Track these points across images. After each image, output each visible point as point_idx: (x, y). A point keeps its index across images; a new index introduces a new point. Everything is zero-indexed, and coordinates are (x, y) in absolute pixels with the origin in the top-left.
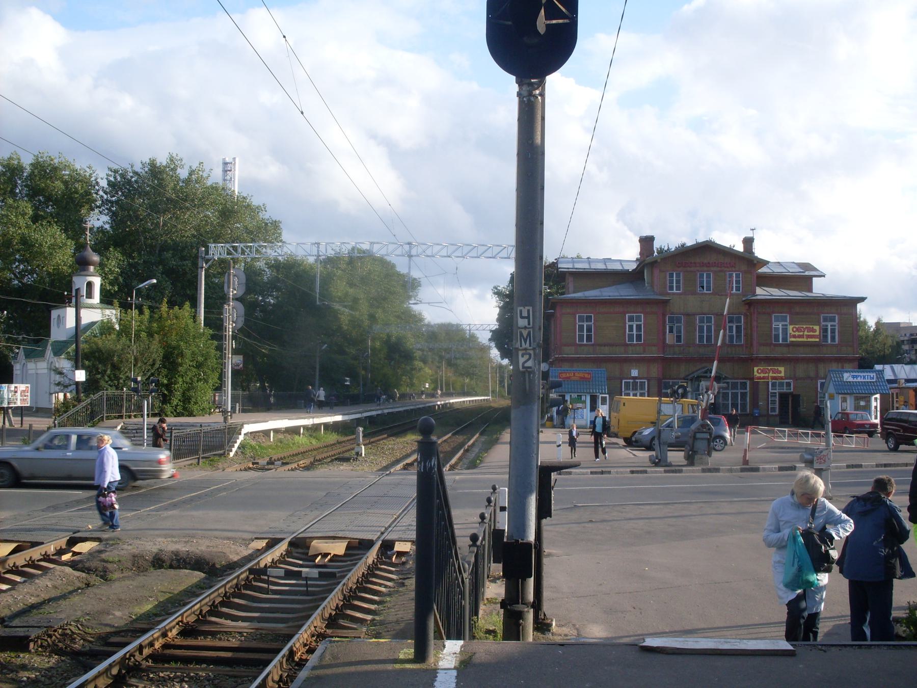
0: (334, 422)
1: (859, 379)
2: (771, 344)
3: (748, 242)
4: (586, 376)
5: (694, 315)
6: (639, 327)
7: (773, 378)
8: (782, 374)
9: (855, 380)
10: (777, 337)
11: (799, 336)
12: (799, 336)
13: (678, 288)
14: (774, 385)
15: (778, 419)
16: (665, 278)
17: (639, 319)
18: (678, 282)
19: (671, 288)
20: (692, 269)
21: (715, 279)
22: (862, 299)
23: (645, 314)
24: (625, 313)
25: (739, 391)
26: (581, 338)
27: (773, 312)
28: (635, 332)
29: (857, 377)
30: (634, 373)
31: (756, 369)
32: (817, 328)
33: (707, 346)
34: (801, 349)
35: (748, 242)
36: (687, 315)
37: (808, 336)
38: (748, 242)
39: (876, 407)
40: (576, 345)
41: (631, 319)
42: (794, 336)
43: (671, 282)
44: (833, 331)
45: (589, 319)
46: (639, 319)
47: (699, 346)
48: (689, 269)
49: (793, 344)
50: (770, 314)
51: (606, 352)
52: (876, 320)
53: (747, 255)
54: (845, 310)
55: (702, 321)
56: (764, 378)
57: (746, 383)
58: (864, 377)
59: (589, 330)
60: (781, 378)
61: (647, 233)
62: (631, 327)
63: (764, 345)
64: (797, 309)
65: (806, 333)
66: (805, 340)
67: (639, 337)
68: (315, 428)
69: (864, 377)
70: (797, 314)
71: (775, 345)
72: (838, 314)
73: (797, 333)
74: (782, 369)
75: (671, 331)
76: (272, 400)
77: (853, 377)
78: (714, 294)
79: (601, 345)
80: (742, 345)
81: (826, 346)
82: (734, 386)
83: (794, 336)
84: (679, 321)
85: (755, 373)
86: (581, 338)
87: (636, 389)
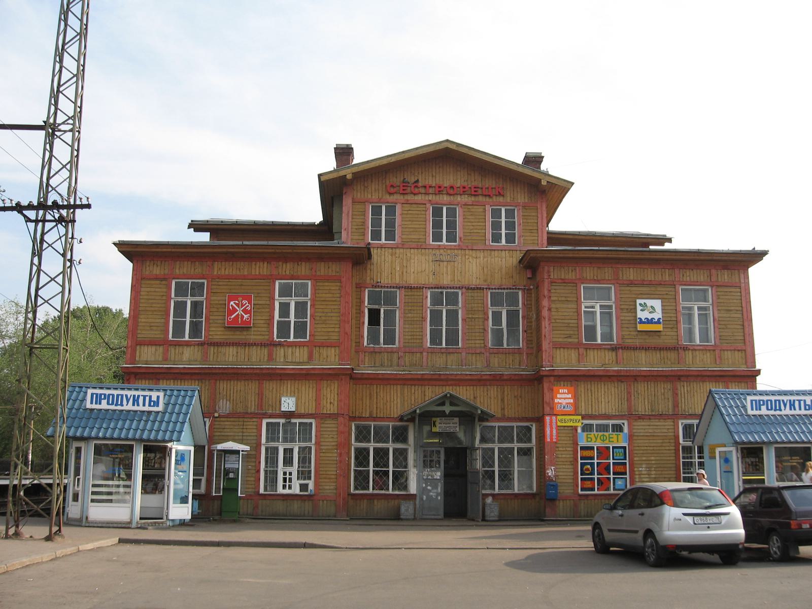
5: (420, 288)
6: (301, 308)
10: (591, 330)
16: (364, 213)
19: (376, 235)
20: (418, 198)
22: (756, 256)
23: (315, 279)
24: (272, 278)
25: (391, 446)
26: (179, 328)
27: (583, 280)
28: (292, 318)
30: (288, 404)
33: (447, 352)
43: (496, 226)
45: (197, 289)
47: (431, 352)
48: (410, 197)
50: (575, 284)
53: (528, 171)
54: (725, 276)
55: (437, 300)
57: (529, 429)
58: (136, 401)
61: (344, 141)
62: (285, 308)
69: (136, 401)
70: (631, 283)
72: (712, 286)
76: (429, 488)
80: (519, 351)
81: (694, 349)
82: (381, 435)
86: (179, 328)
87: (293, 440)
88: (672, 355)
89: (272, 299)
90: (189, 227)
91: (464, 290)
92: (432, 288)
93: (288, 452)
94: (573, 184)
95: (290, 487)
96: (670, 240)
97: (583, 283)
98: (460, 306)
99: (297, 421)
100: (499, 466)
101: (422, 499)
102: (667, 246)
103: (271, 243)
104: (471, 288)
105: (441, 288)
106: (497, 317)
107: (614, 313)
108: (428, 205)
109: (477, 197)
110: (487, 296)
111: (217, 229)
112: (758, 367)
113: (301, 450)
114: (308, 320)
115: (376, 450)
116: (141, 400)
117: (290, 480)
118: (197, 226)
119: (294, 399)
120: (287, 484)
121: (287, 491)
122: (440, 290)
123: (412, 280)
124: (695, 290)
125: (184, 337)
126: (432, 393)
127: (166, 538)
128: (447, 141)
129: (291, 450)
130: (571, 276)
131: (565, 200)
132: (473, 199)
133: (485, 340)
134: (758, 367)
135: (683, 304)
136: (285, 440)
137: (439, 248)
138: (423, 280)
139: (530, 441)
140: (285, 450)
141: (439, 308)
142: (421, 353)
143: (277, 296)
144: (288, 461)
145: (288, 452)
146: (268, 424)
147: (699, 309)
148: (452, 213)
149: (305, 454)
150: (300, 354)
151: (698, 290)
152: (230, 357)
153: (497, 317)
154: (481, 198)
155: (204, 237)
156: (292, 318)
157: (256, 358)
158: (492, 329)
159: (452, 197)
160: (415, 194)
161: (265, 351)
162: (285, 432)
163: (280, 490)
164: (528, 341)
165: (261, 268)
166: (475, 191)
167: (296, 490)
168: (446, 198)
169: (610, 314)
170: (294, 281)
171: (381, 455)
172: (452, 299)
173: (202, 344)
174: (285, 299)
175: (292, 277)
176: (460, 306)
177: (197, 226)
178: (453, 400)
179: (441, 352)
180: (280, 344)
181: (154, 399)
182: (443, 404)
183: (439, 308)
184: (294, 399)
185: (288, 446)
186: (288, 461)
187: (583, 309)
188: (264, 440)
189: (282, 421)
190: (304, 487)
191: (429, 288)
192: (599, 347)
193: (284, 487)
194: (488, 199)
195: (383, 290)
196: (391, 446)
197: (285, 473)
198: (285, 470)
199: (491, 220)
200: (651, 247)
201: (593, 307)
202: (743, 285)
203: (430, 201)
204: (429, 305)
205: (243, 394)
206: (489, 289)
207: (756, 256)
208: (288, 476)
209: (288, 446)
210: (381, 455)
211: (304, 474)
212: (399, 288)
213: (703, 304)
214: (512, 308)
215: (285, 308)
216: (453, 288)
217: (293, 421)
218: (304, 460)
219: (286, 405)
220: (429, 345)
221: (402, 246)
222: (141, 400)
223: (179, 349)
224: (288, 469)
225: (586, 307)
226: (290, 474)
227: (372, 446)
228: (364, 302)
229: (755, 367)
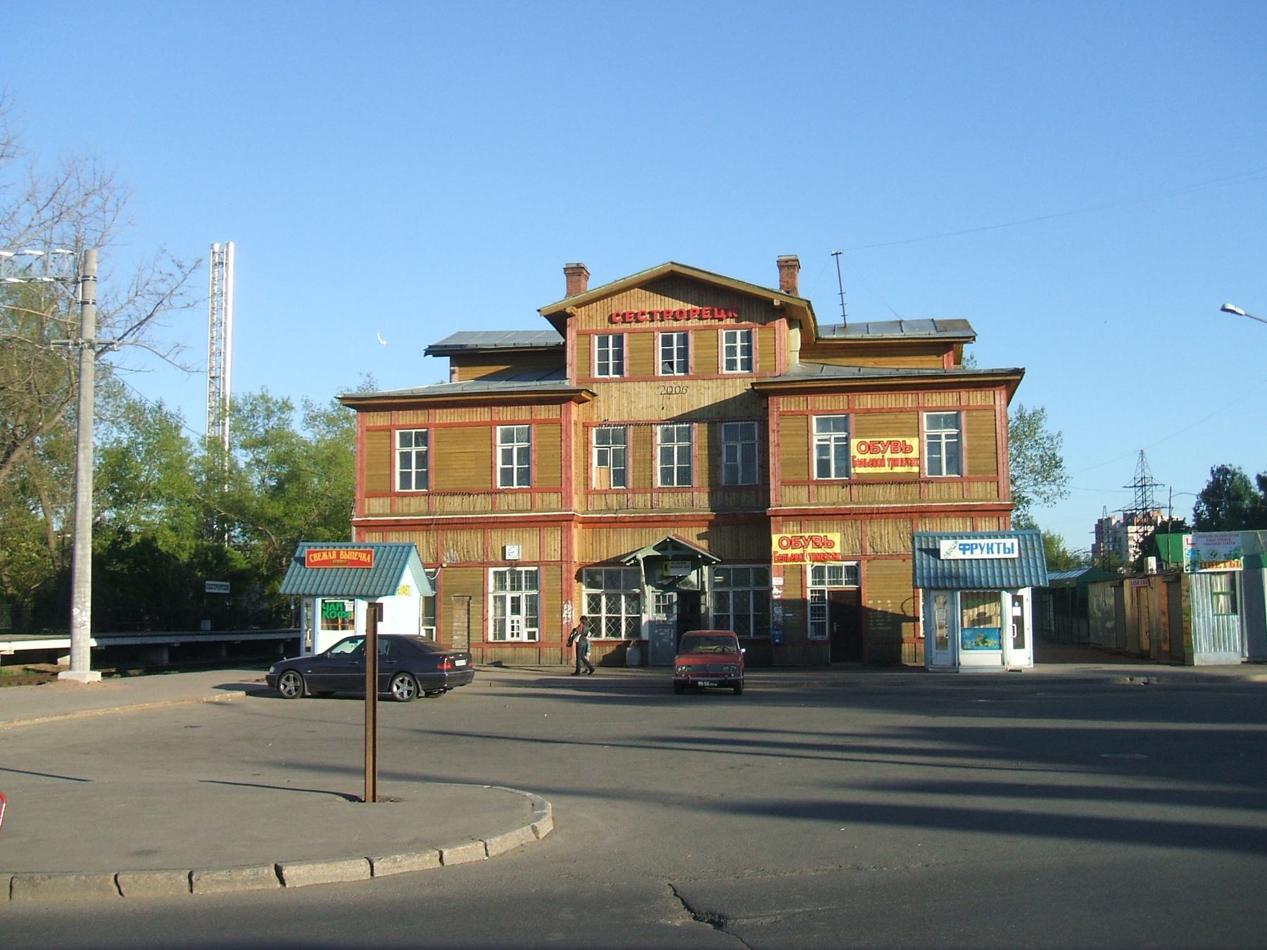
0: (182, 644)
1: (977, 554)
4: (363, 557)
7: (815, 558)
8: (837, 549)
9: (968, 555)
11: (873, 463)
12: (873, 463)
14: (818, 572)
15: (828, 650)
28: (603, 614)
29: (971, 548)
30: (513, 553)
31: (775, 538)
32: (914, 442)
34: (879, 490)
35: (789, 266)
37: (894, 463)
38: (789, 266)
39: (1019, 621)
40: (494, 492)
42: (863, 463)
49: (865, 481)
52: (1203, 481)
56: (794, 558)
58: (990, 549)
60: (835, 557)
65: (888, 455)
66: (886, 469)
69: (990, 549)
73: (868, 457)
74: (836, 537)
75: (602, 460)
77: (964, 548)
83: (863, 463)
85: (775, 547)
87: (519, 588)
88: (914, 489)
89: (493, 445)
90: (427, 353)
93: (516, 601)
101: (654, 646)
116: (995, 548)
121: (515, 639)
123: (642, 416)
126: (661, 535)
136: (513, 588)
137: (606, 381)
138: (654, 415)
140: (513, 599)
141: (669, 445)
144: (516, 610)
145: (516, 601)
146: (495, 573)
148: (684, 339)
149: (533, 601)
150: (523, 500)
152: (455, 506)
157: (479, 506)
158: (727, 466)
161: (489, 498)
163: (508, 638)
165: (907, 400)
167: (524, 638)
172: (620, 438)
174: (507, 446)
179: (673, 491)
181: (1009, 545)
183: (669, 445)
185: (516, 594)
186: (516, 610)
190: (531, 635)
199: (725, 345)
205: (470, 542)
209: (516, 594)
211: (532, 622)
217: (518, 569)
218: (533, 608)
221: (630, 380)
222: (995, 548)
223: (406, 500)
224: (516, 617)
227: (523, 594)
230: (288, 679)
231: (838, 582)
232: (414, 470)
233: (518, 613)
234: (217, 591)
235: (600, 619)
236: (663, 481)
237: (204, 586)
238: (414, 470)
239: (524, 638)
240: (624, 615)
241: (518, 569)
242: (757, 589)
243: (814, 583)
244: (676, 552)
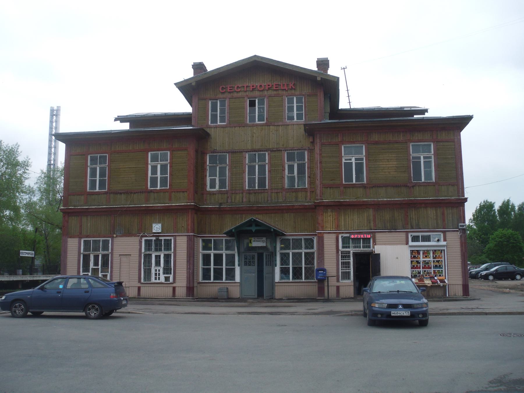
2: (342, 184)
3: (323, 64)
13: (222, 120)
17: (164, 158)
18: (222, 111)
19: (214, 120)
20: (240, 94)
21: (269, 106)
22: (462, 122)
23: (172, 151)
24: (147, 151)
27: (342, 142)
28: (159, 175)
34: (382, 191)
36: (233, 152)
41: (155, 159)
44: (428, 164)
46: (164, 158)
47: (249, 192)
48: (235, 95)
50: (338, 145)
51: (122, 202)
53: (202, 76)
54: (443, 136)
59: (102, 174)
61: (322, 56)
62: (154, 168)
63: (331, 187)
64: (375, 137)
67: (164, 181)
68: (266, 259)
70: (376, 143)
71: (346, 187)
72: (434, 142)
78: (230, 125)
79: (116, 193)
84: (223, 160)
87: (160, 250)
90: (116, 120)
91: (269, 152)
92: (249, 152)
93: (158, 258)
94: (175, 84)
95: (159, 278)
96: (426, 111)
97: (343, 144)
98: (267, 162)
99: (163, 238)
100: (293, 264)
102: (427, 115)
103: (357, 120)
104: (274, 151)
105: (254, 151)
106: (291, 168)
107: (433, 161)
108: (246, 98)
109: (232, 94)
110: (284, 155)
111: (134, 120)
112: (466, 196)
113: (103, 256)
114: (168, 176)
115: (215, 255)
117: (159, 274)
118: (122, 119)
119: (160, 225)
120: (157, 277)
121: (157, 281)
122: (254, 153)
124: (354, 146)
125: (96, 189)
126: (246, 219)
127: (255, 311)
128: (255, 56)
129: (160, 256)
130: (401, 138)
131: (340, 88)
132: (275, 92)
133: (283, 183)
134: (466, 196)
135: (413, 155)
136: (156, 250)
139: (312, 248)
140: (156, 256)
142: (242, 193)
143: (149, 162)
144: (158, 263)
145: (158, 258)
147: (424, 158)
151: (425, 145)
153: (291, 168)
154: (280, 92)
155: (126, 126)
156: (159, 175)
158: (288, 177)
159: (261, 93)
160: (237, 92)
162: (156, 245)
164: (310, 183)
166: (276, 87)
168: (257, 93)
169: (430, 162)
170: (159, 152)
171: (218, 259)
173: (106, 193)
175: (159, 150)
176: (267, 162)
177: (122, 119)
178: (257, 224)
180: (151, 191)
182: (251, 225)
184: (160, 225)
186: (158, 263)
187: (344, 161)
188: (143, 250)
189: (154, 238)
190: (167, 279)
191: (247, 152)
192: (354, 186)
193: (156, 279)
194: (284, 92)
195: (218, 154)
196: (224, 253)
197: (156, 270)
198: (156, 268)
200: (415, 116)
201: (350, 160)
202: (456, 140)
203: (247, 95)
204: (247, 162)
206: (286, 150)
207: (462, 122)
208: (157, 272)
209: (158, 253)
210: (297, 257)
212: (228, 152)
213: (426, 154)
214: (301, 162)
215: (154, 168)
216: (223, 152)
217: (160, 238)
219: (156, 229)
220: (247, 188)
224: (158, 268)
225: (345, 160)
226: (159, 271)
227: (212, 252)
228: (206, 163)
229: (464, 196)
230: (20, 306)
231: (357, 247)
232: (212, 267)
233: (160, 265)
234: (27, 255)
235: (210, 269)
236: (204, 278)
237: (19, 253)
238: (212, 267)
239: (162, 279)
240: (291, 266)
241: (160, 238)
242: (300, 251)
243: (343, 247)
244: (258, 228)
